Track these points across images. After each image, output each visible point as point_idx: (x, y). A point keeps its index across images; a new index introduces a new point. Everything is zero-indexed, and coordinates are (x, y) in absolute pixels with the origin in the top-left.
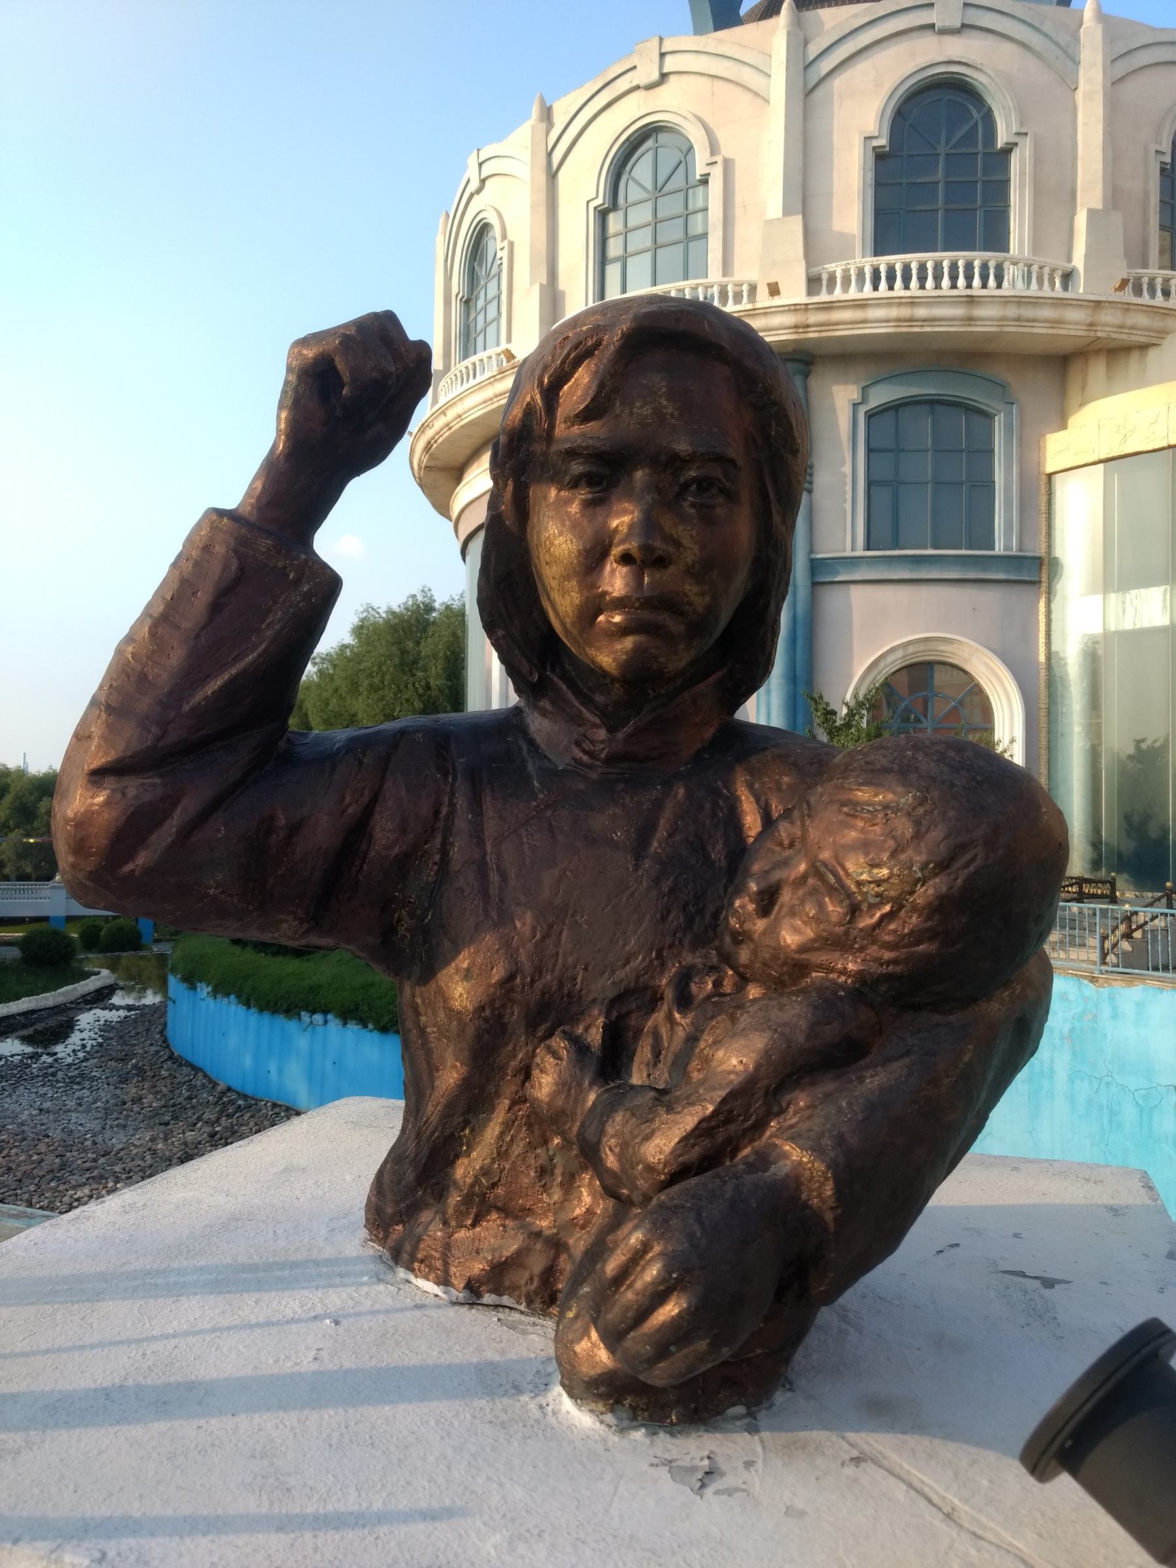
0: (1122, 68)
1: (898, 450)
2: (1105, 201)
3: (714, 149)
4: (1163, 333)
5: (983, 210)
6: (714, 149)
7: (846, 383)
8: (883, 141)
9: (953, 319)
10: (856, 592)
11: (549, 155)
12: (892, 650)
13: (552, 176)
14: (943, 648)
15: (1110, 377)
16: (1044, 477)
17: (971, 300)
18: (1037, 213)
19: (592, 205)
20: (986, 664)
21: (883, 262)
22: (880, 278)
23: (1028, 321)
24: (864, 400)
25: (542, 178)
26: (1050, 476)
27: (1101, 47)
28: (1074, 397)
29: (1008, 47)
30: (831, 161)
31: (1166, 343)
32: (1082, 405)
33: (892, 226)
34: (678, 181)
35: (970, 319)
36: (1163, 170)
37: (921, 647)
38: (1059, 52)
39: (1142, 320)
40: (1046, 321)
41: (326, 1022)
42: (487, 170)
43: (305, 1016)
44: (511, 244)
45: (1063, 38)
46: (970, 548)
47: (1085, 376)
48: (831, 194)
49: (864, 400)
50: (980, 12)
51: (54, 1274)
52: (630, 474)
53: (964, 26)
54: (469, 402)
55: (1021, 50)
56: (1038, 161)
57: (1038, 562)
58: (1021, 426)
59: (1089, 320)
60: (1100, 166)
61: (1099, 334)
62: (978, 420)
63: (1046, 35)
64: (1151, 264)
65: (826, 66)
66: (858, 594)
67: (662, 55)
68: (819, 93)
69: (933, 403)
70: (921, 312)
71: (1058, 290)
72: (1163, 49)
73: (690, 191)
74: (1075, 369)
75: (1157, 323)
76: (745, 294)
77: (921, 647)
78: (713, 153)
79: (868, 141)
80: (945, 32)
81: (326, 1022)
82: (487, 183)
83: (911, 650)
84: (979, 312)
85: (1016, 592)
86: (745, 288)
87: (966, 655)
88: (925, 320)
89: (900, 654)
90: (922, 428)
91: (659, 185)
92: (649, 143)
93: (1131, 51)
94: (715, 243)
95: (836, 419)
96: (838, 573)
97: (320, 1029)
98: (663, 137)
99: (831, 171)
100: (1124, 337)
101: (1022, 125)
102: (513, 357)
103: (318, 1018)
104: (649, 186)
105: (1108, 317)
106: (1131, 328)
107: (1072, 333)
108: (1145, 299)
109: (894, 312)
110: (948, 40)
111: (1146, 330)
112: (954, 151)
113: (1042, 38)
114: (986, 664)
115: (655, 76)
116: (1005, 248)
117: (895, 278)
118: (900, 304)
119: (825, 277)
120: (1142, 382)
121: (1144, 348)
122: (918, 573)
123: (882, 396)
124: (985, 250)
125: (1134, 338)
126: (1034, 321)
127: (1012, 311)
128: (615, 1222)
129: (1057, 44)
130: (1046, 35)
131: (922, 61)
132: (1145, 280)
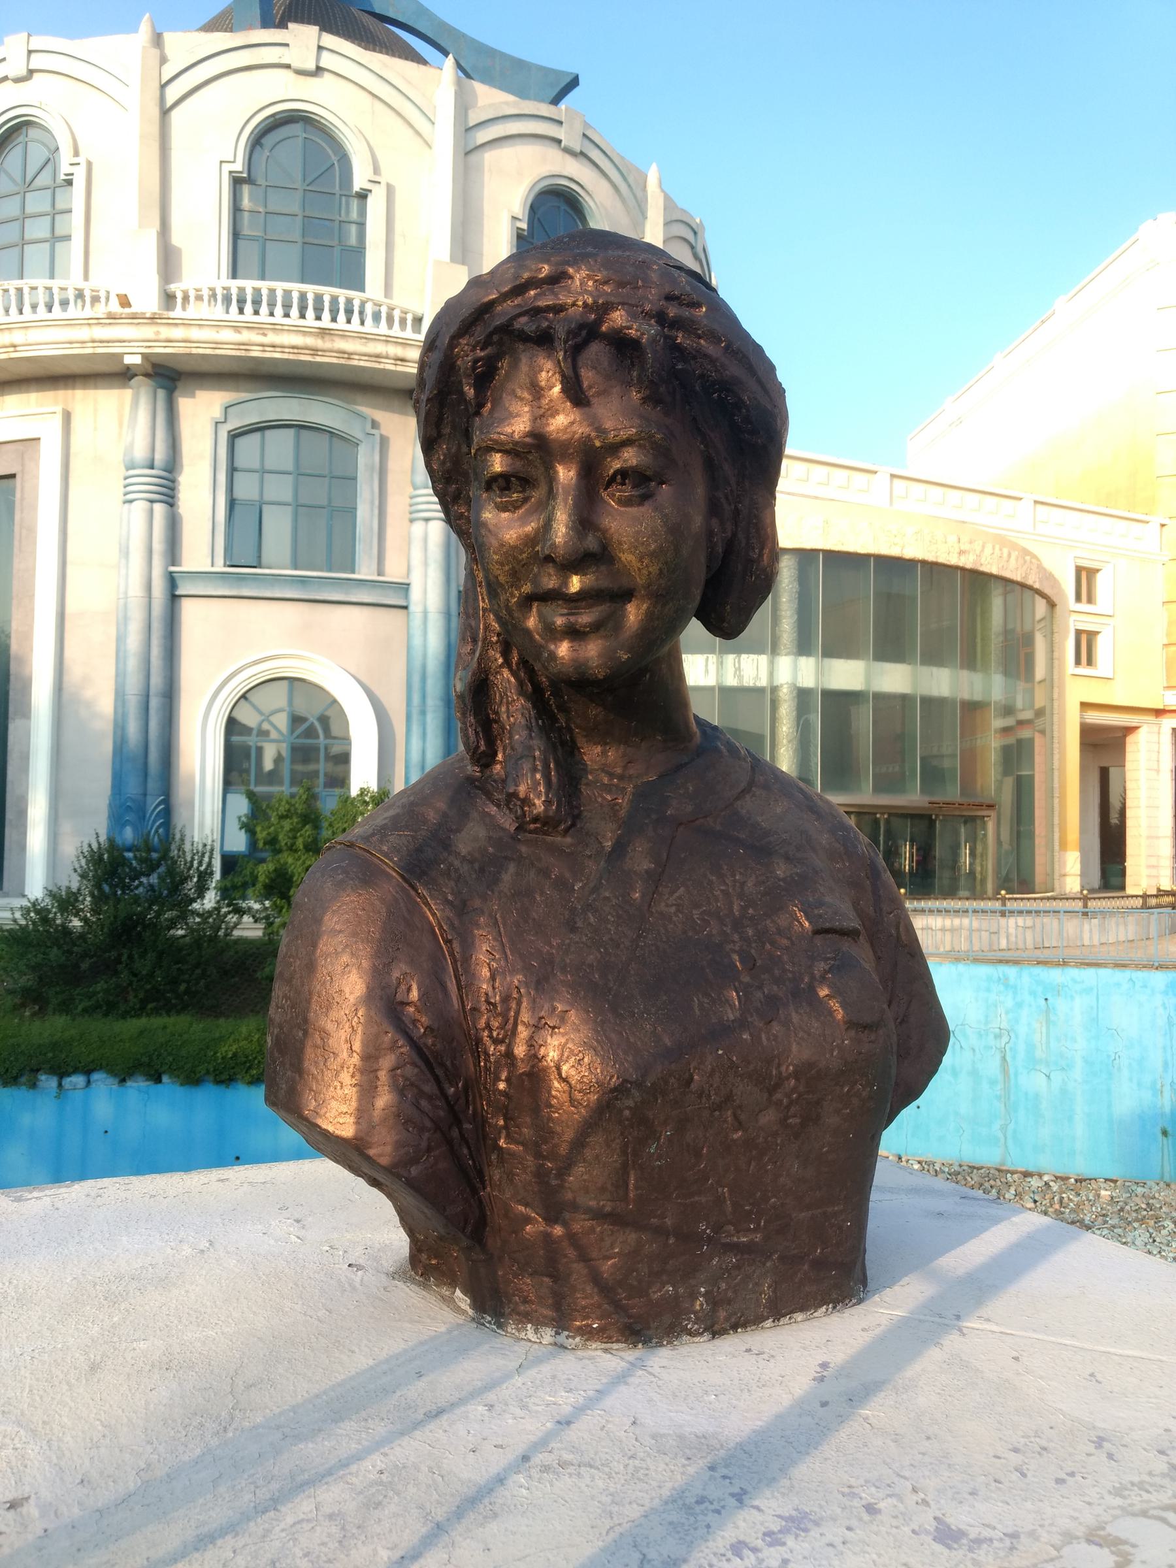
3: (376, 170)
5: (339, 248)
6: (376, 170)
8: (239, 166)
11: (163, 87)
13: (165, 112)
19: (227, 168)
25: (155, 112)
30: (482, 225)
33: (245, 247)
34: (44, 179)
41: (89, 1082)
42: (37, 62)
43: (48, 1082)
44: (89, 165)
46: (296, 569)
48: (482, 255)
52: (484, 525)
54: (35, 335)
65: (482, 136)
67: (30, 52)
68: (473, 158)
69: (301, 427)
71: (326, 322)
73: (344, 199)
76: (409, 322)
78: (76, 154)
80: (568, 151)
81: (89, 1082)
82: (36, 75)
86: (409, 317)
91: (28, 179)
92: (296, 129)
94: (77, 243)
97: (78, 1095)
98: (33, 133)
102: (129, 305)
103: (78, 1080)
104: (19, 179)
109: (298, 340)
112: (309, 188)
115: (24, 72)
116: (362, 289)
117: (245, 301)
119: (179, 296)
124: (303, 282)
128: (714, 1310)
129: (635, 197)
131: (556, 170)
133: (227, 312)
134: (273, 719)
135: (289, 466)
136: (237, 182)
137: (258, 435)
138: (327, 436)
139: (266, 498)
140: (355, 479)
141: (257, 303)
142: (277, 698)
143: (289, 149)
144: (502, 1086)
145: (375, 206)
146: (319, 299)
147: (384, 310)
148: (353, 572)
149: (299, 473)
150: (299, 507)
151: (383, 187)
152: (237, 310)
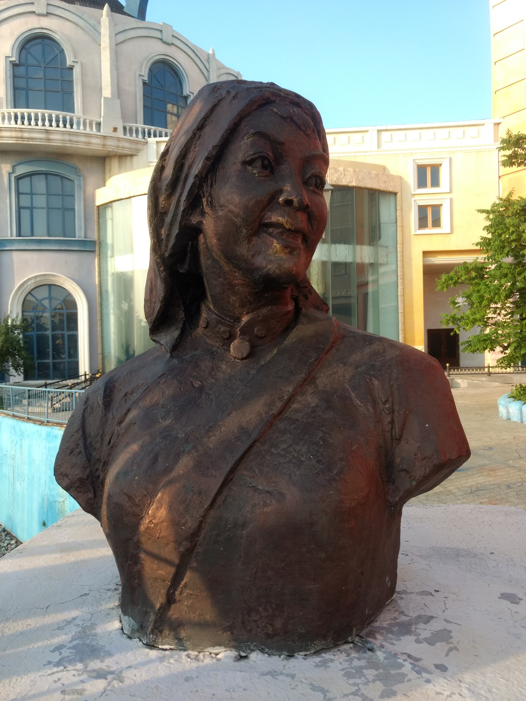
0: (121, 37)
1: (32, 194)
2: (112, 94)
4: (138, 151)
7: (6, 163)
8: (13, 59)
9: (41, 139)
10: (15, 254)
12: (29, 279)
14: (52, 278)
15: (120, 167)
16: (96, 208)
17: (47, 131)
18: (84, 97)
20: (71, 285)
21: (19, 111)
22: (18, 118)
23: (75, 142)
24: (13, 171)
26: (98, 207)
27: (108, 28)
28: (107, 176)
29: (69, 24)
31: (140, 154)
32: (109, 178)
35: (49, 140)
36: (144, 83)
37: (42, 278)
38: (91, 28)
39: (127, 145)
40: (83, 142)
45: (93, 22)
46: (65, 237)
47: (111, 166)
49: (13, 171)
50: (55, 8)
51: (29, 675)
53: (48, 13)
55: (75, 26)
56: (83, 74)
57: (93, 243)
58: (85, 185)
59: (102, 143)
60: (109, 79)
61: (109, 149)
62: (66, 182)
63: (85, 20)
64: (138, 121)
66: (15, 255)
69: (46, 174)
70: (26, 135)
72: (143, 30)
74: (107, 161)
75: (134, 146)
77: (42, 278)
79: (7, 58)
80: (40, 15)
83: (38, 279)
84: (52, 137)
85: (85, 255)
87: (62, 282)
88: (29, 139)
89: (33, 281)
90: (40, 184)
93: (125, 30)
95: (3, 180)
96: (6, 246)
99: (111, 58)
100: (120, 151)
101: (75, 58)
105: (109, 142)
106: (122, 148)
107: (96, 148)
108: (128, 137)
109: (14, 134)
110: (42, 18)
111: (129, 148)
112: (47, 66)
113: (83, 21)
114: (71, 285)
117: (31, 119)
118: (16, 131)
120: (132, 169)
121: (132, 156)
122: (39, 246)
123: (22, 170)
125: (125, 152)
126: (78, 142)
127: (67, 137)
130: (85, 20)
131: (30, 26)
132: (134, 128)
133: (4, 124)
134: (43, 302)
135: (44, 192)
136: (14, 65)
137: (28, 179)
138: (59, 178)
139: (61, 207)
140: (74, 196)
141: (30, 119)
142: (43, 293)
143: (36, 49)
144: (448, 365)
145: (77, 72)
146: (36, 115)
147: (82, 120)
148: (75, 237)
149: (48, 194)
150: (49, 208)
151: (79, 63)
152: (15, 123)
